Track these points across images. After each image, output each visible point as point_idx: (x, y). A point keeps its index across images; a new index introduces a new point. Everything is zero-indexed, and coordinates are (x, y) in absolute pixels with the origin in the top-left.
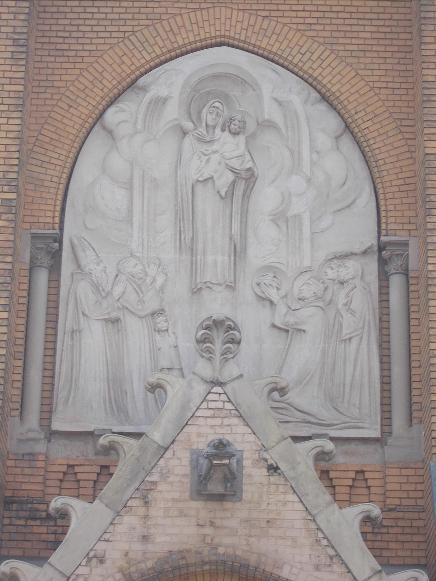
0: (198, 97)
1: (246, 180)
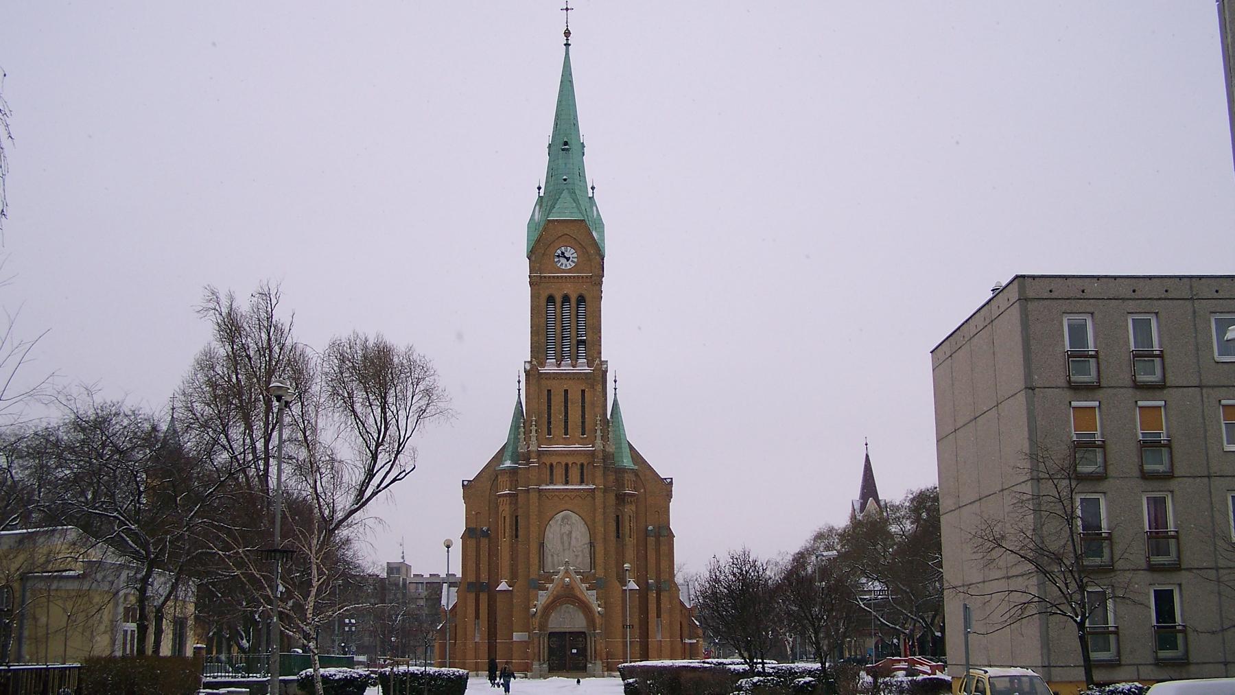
0: (563, 519)
1: (571, 532)
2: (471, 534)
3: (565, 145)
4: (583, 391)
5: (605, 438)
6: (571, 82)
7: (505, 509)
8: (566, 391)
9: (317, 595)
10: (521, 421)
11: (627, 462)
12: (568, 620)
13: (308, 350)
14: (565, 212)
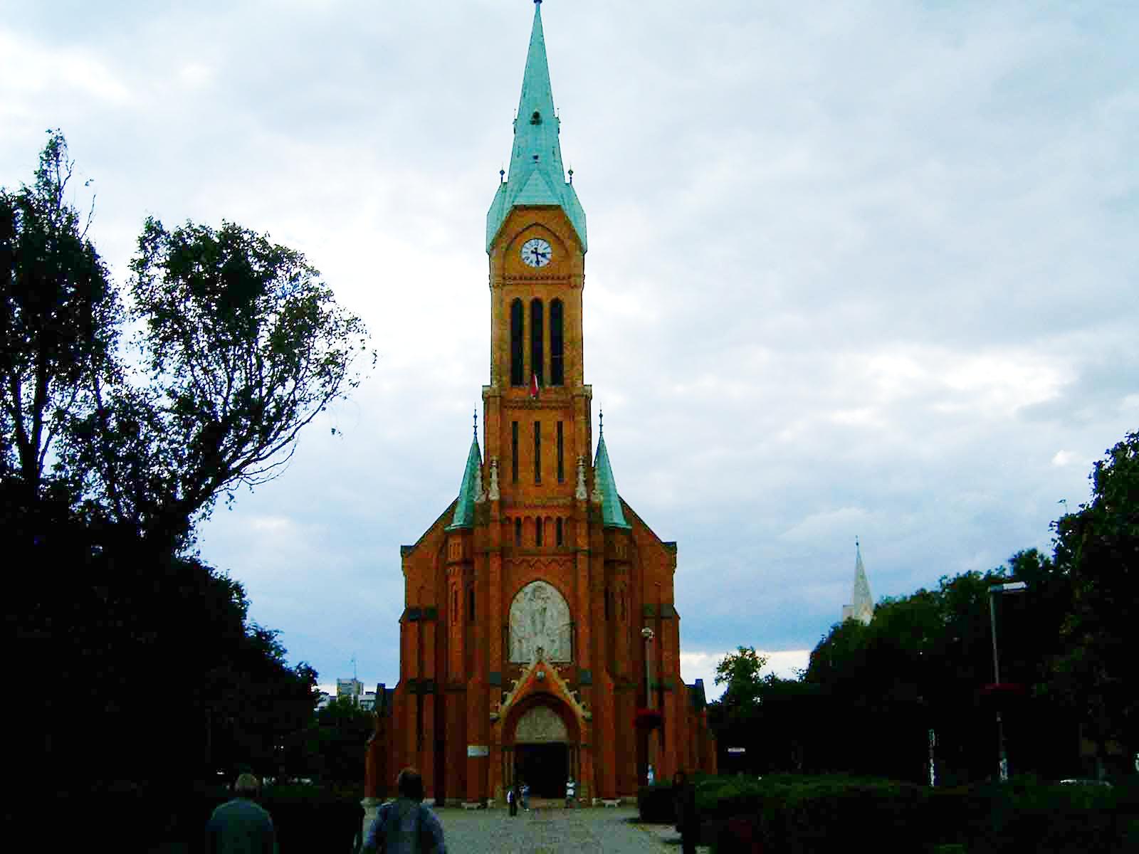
0: (535, 590)
1: (545, 609)
2: (413, 618)
3: (537, 118)
4: (560, 425)
5: (589, 483)
6: (542, 44)
7: (456, 580)
8: (537, 424)
9: (229, 806)
10: (479, 468)
11: (619, 519)
12: (544, 729)
13: (175, 231)
14: (536, 194)
